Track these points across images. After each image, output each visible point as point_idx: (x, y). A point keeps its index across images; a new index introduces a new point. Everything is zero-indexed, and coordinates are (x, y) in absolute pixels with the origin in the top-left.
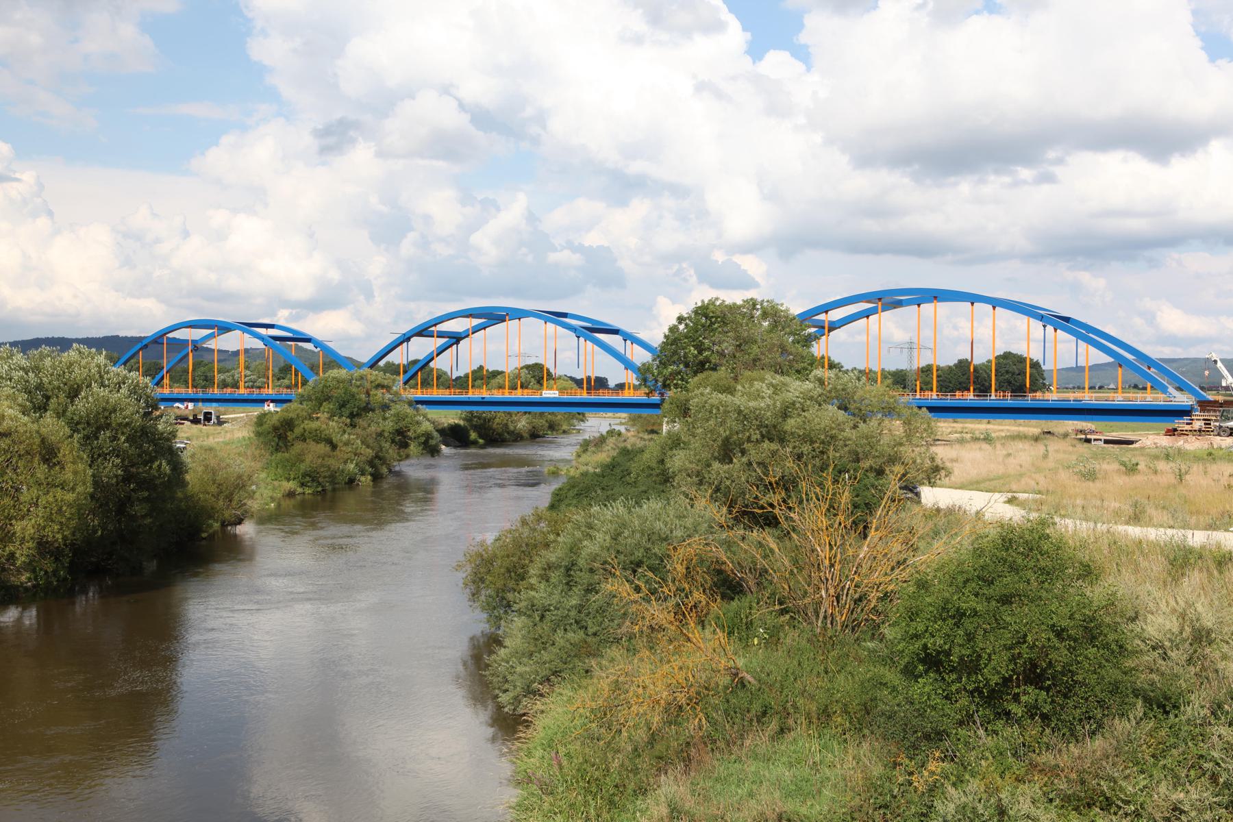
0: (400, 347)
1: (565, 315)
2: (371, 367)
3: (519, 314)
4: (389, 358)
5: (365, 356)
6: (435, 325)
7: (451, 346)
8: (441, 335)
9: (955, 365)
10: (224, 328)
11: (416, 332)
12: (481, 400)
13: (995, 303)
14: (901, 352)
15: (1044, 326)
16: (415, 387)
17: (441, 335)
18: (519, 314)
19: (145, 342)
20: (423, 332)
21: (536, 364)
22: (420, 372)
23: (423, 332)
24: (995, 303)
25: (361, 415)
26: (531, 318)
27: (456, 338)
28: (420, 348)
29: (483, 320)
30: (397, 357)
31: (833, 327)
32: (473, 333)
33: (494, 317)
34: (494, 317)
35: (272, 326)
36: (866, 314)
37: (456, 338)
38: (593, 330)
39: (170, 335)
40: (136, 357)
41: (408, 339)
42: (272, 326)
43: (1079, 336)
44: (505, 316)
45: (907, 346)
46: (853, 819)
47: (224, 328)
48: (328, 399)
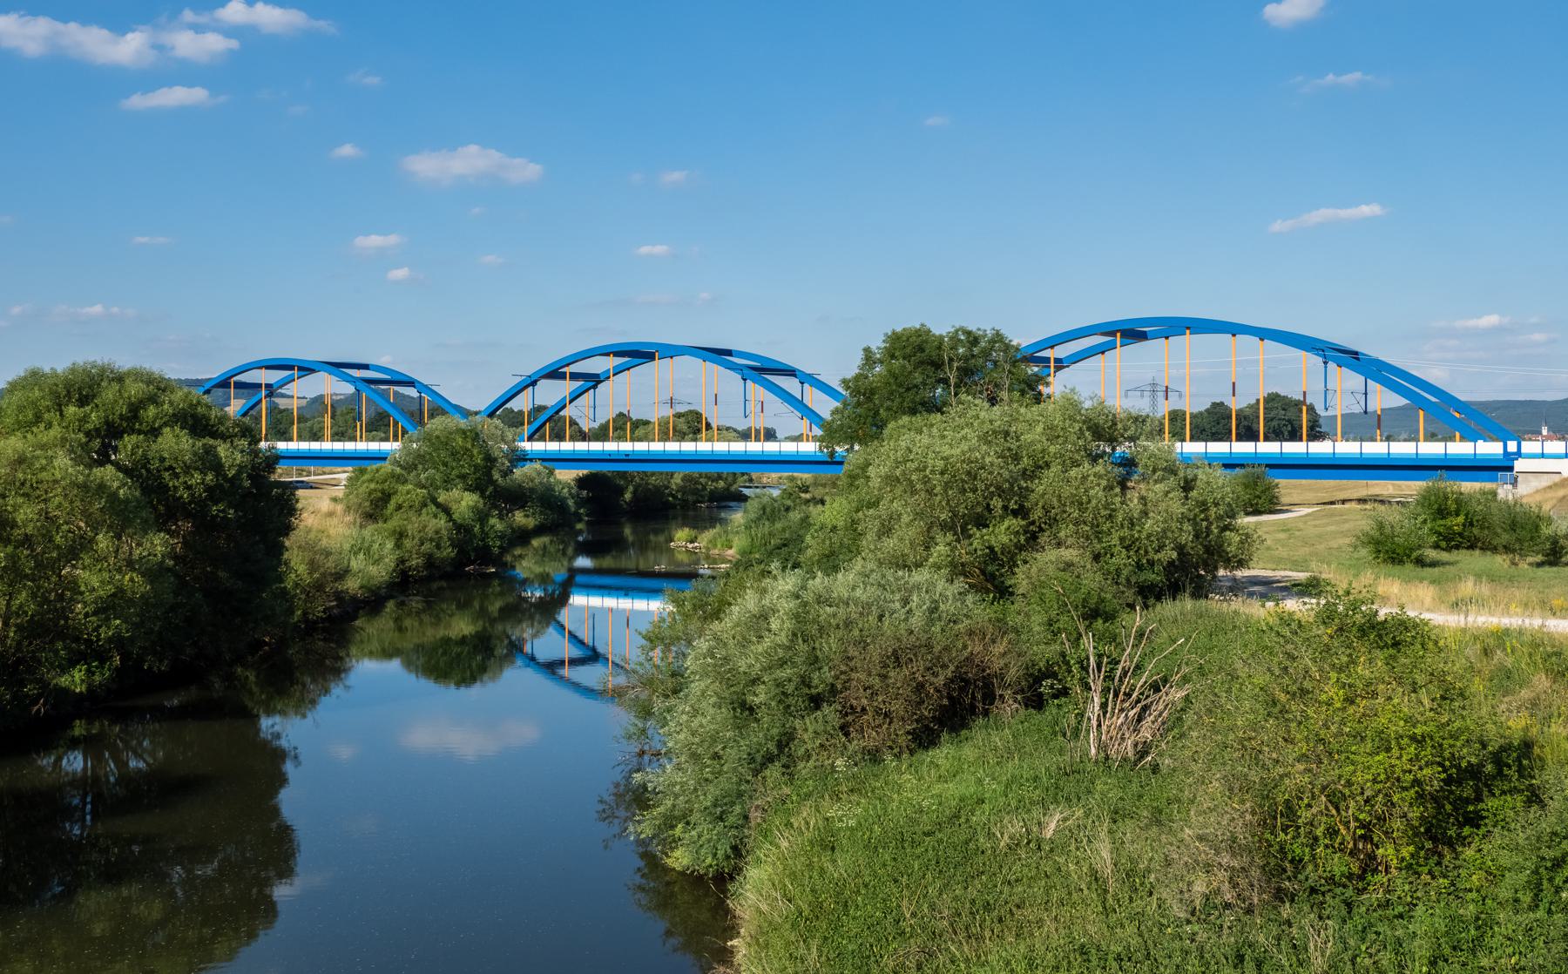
0: (586, 394)
1: (729, 353)
2: (491, 415)
3: (672, 351)
4: (512, 405)
5: (479, 401)
6: (568, 365)
7: (589, 389)
8: (575, 376)
9: (1207, 410)
10: (306, 369)
11: (545, 373)
12: (624, 457)
13: (1263, 334)
14: (1142, 396)
15: (1325, 363)
16: (543, 439)
17: (575, 376)
18: (672, 351)
19: (207, 386)
20: (555, 374)
21: (691, 411)
22: (553, 424)
23: (555, 374)
24: (1263, 334)
25: (1246, 486)
26: (1463, 398)
27: (595, 380)
28: (550, 394)
29: (627, 359)
30: (522, 403)
31: (1060, 364)
32: (614, 375)
33: (640, 354)
34: (640, 354)
35: (366, 367)
36: (1101, 350)
37: (595, 380)
38: (764, 370)
39: (235, 378)
40: (258, 407)
41: (534, 383)
42: (366, 367)
43: (1368, 375)
44: (654, 353)
45: (1149, 388)
46: (1031, 965)
47: (306, 369)
48: (1174, 472)
